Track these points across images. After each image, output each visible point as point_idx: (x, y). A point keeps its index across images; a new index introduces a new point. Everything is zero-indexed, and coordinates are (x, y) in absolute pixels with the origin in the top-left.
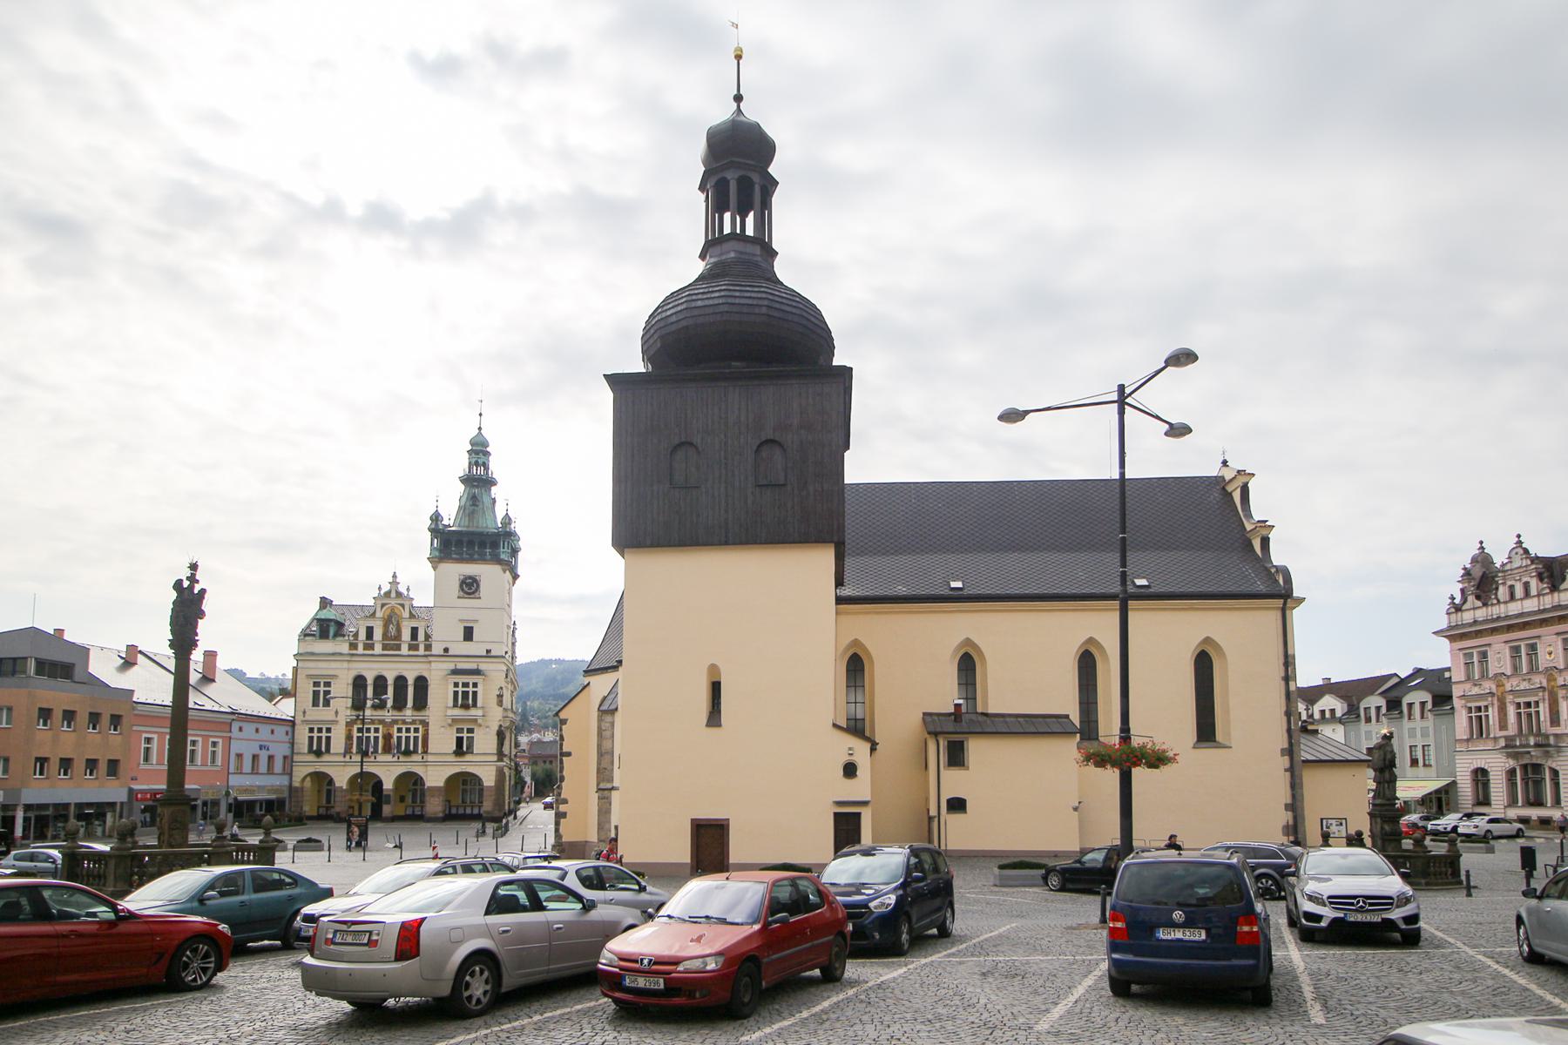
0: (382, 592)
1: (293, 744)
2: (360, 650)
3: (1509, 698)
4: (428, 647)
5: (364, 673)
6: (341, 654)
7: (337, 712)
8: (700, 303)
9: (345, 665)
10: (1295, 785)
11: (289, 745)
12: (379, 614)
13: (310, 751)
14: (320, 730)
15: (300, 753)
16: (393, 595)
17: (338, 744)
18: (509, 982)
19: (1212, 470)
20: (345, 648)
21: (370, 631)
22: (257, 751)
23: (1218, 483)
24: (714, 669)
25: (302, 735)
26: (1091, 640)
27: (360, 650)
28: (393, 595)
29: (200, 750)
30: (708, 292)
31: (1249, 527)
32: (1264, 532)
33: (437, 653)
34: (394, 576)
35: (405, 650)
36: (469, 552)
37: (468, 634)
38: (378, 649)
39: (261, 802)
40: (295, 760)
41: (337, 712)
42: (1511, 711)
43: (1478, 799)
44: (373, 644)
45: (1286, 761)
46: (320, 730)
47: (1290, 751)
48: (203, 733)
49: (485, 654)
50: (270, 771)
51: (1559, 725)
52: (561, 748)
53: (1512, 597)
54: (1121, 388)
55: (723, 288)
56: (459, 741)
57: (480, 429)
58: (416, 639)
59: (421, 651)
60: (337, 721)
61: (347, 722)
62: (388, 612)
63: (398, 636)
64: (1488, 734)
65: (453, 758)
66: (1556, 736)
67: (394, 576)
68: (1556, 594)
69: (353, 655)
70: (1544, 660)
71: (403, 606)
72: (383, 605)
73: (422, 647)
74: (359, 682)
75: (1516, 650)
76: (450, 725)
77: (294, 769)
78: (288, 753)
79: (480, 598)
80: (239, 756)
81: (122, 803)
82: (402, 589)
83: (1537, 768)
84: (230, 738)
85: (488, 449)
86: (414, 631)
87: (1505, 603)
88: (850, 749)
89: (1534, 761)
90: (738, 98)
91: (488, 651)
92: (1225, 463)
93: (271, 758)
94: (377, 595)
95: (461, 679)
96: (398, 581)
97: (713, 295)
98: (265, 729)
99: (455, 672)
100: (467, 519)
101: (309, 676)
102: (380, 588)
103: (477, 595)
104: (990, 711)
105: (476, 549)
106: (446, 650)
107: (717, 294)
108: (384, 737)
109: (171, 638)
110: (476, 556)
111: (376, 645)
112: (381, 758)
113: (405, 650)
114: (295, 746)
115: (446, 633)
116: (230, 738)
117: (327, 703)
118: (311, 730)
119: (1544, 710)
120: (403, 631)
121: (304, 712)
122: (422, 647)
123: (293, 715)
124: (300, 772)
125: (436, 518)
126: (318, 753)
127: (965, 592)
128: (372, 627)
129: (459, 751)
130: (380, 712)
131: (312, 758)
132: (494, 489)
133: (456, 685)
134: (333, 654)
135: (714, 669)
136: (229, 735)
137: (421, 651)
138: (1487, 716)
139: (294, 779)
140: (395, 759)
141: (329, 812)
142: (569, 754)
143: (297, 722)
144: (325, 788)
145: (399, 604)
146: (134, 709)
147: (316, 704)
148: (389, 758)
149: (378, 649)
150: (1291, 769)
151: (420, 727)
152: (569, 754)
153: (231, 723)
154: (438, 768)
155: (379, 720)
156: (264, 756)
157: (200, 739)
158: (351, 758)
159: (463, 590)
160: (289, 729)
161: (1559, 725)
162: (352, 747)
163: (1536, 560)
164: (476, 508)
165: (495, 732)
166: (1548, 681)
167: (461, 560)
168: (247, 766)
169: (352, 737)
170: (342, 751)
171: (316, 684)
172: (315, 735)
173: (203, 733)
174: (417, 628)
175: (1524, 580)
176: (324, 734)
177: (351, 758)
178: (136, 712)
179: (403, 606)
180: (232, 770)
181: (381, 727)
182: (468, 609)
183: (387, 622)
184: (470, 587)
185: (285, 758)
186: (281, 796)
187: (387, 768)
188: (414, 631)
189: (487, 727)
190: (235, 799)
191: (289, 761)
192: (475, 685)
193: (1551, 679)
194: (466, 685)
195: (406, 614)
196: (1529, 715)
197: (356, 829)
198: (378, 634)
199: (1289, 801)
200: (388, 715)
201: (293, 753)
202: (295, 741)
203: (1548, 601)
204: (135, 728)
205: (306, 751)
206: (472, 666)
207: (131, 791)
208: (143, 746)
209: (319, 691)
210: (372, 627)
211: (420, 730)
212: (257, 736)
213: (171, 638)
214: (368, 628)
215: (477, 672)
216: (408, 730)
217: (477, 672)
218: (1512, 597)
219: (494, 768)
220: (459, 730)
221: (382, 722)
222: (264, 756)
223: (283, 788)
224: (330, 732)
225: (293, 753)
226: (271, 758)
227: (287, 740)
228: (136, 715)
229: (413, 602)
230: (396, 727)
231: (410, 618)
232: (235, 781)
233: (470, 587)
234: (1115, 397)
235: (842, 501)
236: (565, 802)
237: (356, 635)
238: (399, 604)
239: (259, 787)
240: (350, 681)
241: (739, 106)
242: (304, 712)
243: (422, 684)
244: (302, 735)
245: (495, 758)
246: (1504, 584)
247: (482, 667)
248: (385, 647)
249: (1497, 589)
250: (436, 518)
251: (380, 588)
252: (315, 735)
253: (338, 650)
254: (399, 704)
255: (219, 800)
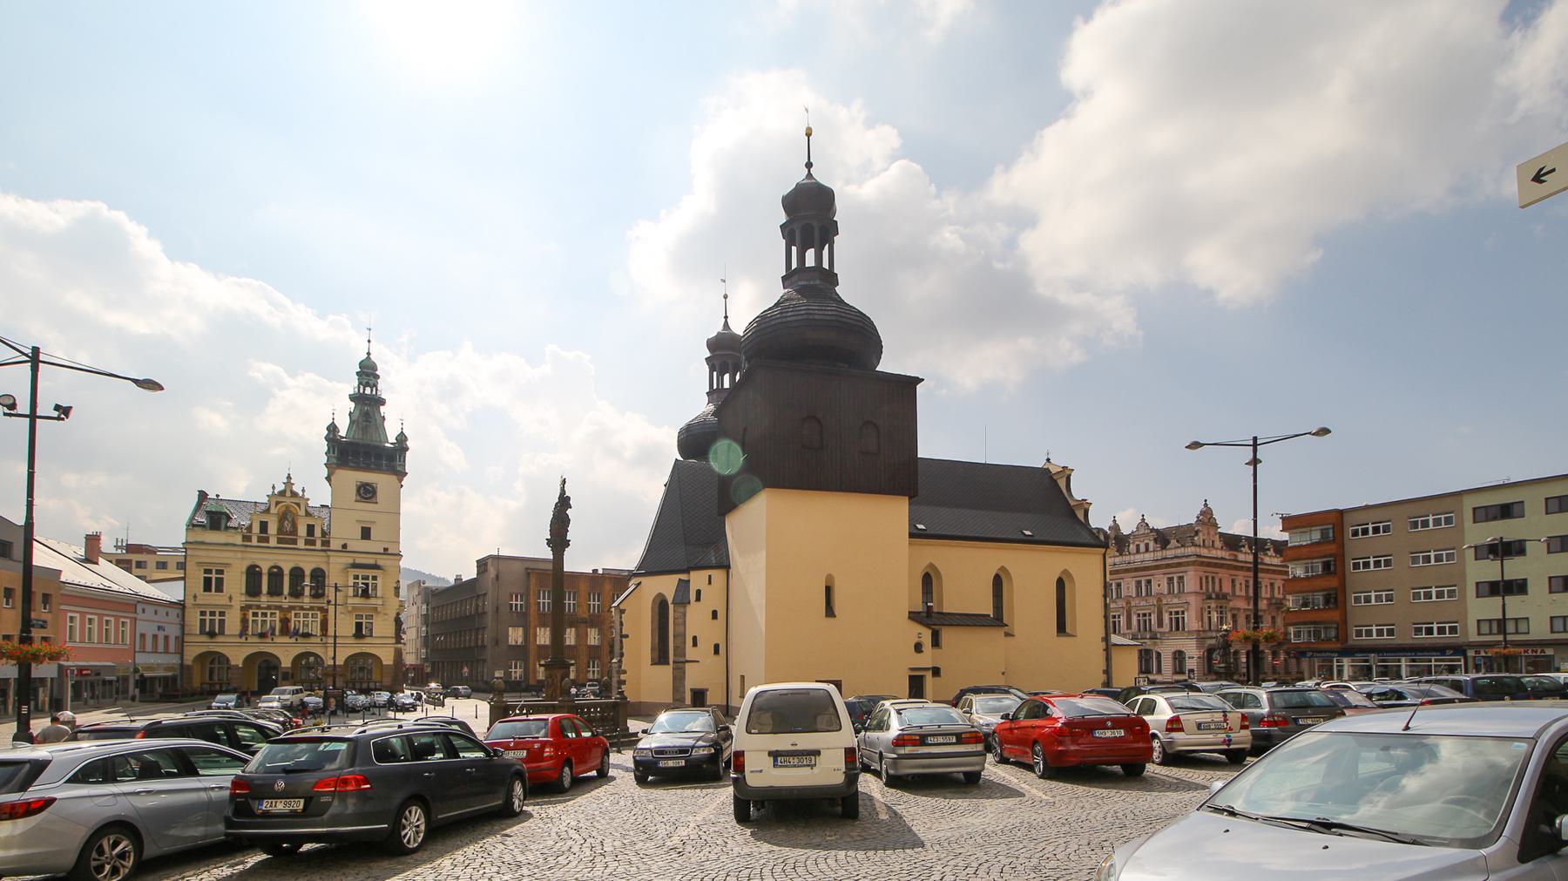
0: (276, 492)
1: (183, 626)
2: (255, 542)
3: (1134, 610)
4: (326, 543)
5: (301, 565)
6: (235, 545)
7: (231, 598)
8: (816, 317)
9: (239, 555)
10: (1108, 659)
11: (179, 626)
12: (273, 510)
13: (202, 632)
14: (213, 614)
15: (192, 634)
16: (288, 494)
17: (233, 623)
18: (150, 851)
19: (1040, 463)
20: (238, 540)
21: (264, 527)
22: (157, 632)
23: (1044, 473)
24: (830, 578)
25: (193, 619)
26: (1003, 568)
27: (255, 542)
28: (288, 494)
29: (96, 628)
30: (822, 310)
31: (1072, 503)
32: (1086, 506)
33: (334, 549)
34: (289, 477)
35: (301, 544)
36: (366, 462)
37: (366, 534)
38: (273, 542)
39: (160, 678)
40: (185, 640)
41: (231, 598)
42: (1134, 619)
43: (1175, 669)
44: (268, 538)
45: (1103, 645)
46: (213, 614)
47: (1106, 639)
48: (114, 613)
49: (382, 551)
50: (166, 651)
51: (1162, 627)
52: (621, 632)
53: (1138, 551)
54: (1255, 439)
55: (833, 308)
56: (359, 626)
57: (726, 317)
58: (313, 536)
59: (318, 546)
60: (231, 606)
61: (242, 607)
62: (284, 509)
63: (294, 531)
64: (1184, 629)
65: (353, 641)
66: (1161, 633)
67: (289, 477)
68: (1164, 551)
69: (247, 546)
70: (1155, 589)
71: (298, 505)
72: (277, 503)
73: (319, 543)
74: (253, 574)
75: (1139, 583)
76: (349, 612)
77: (185, 648)
78: (178, 633)
79: (377, 503)
80: (143, 636)
81: (52, 679)
82: (297, 489)
83: (1148, 652)
84: (136, 619)
85: (377, 373)
86: (311, 529)
87: (1134, 554)
88: (920, 634)
89: (1147, 647)
90: (809, 165)
91: (386, 549)
92: (1048, 460)
93: (166, 638)
94: (270, 493)
95: (361, 572)
96: (292, 481)
97: (826, 313)
98: (162, 611)
99: (355, 566)
100: (361, 432)
101: (199, 564)
102: (274, 487)
103: (373, 500)
104: (944, 611)
105: (373, 460)
106: (345, 546)
107: (803, 312)
108: (281, 621)
109: (549, 537)
110: (372, 466)
111: (271, 539)
112: (279, 640)
113: (301, 544)
114: (186, 628)
115: (344, 530)
116: (136, 619)
117: (219, 589)
118: (203, 613)
119: (1154, 618)
120: (299, 527)
121: (195, 597)
122: (319, 543)
123: (182, 599)
124: (191, 654)
125: (332, 428)
126: (212, 634)
127: (928, 532)
128: (267, 522)
129: (359, 633)
130: (276, 599)
131: (204, 638)
132: (382, 409)
133: (356, 577)
134: (226, 544)
135: (830, 578)
136: (133, 615)
137: (318, 546)
138: (1119, 621)
139: (185, 657)
140: (293, 640)
141: (213, 689)
142: (627, 636)
143: (186, 605)
144: (208, 666)
145: (276, 505)
146: (60, 589)
147: (207, 587)
148: (286, 639)
149: (273, 542)
150: (1107, 650)
151: (319, 613)
152: (627, 636)
153: (136, 605)
154: (384, 649)
155: (276, 606)
156: (161, 635)
157: (96, 617)
158: (246, 639)
159: (360, 495)
160: (179, 611)
161: (1162, 627)
162: (247, 630)
163: (1153, 530)
164: (368, 423)
165: (393, 619)
166: (1127, 603)
167: (358, 468)
168: (149, 647)
169: (248, 620)
170: (238, 632)
171: (208, 571)
172: (208, 617)
173: (114, 613)
174: (313, 526)
175: (1146, 541)
176: (217, 618)
177: (246, 639)
178: (62, 592)
179: (298, 505)
180: (137, 649)
181: (277, 612)
182: (365, 511)
183: (282, 518)
184: (367, 493)
185: (177, 638)
186: (175, 673)
187: (285, 648)
188: (311, 529)
189: (386, 614)
190: (142, 676)
191: (181, 642)
192: (375, 578)
193: (1159, 600)
194: (367, 578)
195: (302, 513)
196: (1145, 621)
197: (332, 700)
198: (273, 529)
199: (1105, 668)
200: (286, 601)
201: (183, 633)
202: (186, 623)
203: (1159, 555)
204: (62, 607)
205: (198, 633)
206: (371, 562)
207: (60, 667)
208: (69, 624)
209: (211, 578)
210: (267, 522)
211: (278, 614)
212: (156, 618)
213: (549, 537)
214: (261, 522)
215: (376, 567)
216: (264, 615)
217: (376, 567)
218: (1138, 551)
219: (393, 650)
220: (358, 616)
221: (279, 608)
222: (161, 635)
223: (175, 666)
224: (224, 616)
225: (183, 633)
226: (166, 638)
227: (177, 622)
228: (62, 595)
229: (309, 502)
230: (293, 612)
231: (306, 516)
232: (141, 659)
233: (367, 493)
234: (1251, 443)
235: (915, 473)
236: (625, 672)
237: (250, 528)
238: (276, 505)
239: (158, 665)
240: (244, 570)
241: (809, 171)
242: (195, 597)
243: (319, 576)
244: (193, 619)
245: (394, 641)
246: (1133, 543)
247: (380, 563)
248: (280, 541)
249: (1129, 546)
250: (332, 428)
251: (274, 487)
252: (208, 617)
253: (230, 540)
254: (296, 593)
255: (128, 676)
